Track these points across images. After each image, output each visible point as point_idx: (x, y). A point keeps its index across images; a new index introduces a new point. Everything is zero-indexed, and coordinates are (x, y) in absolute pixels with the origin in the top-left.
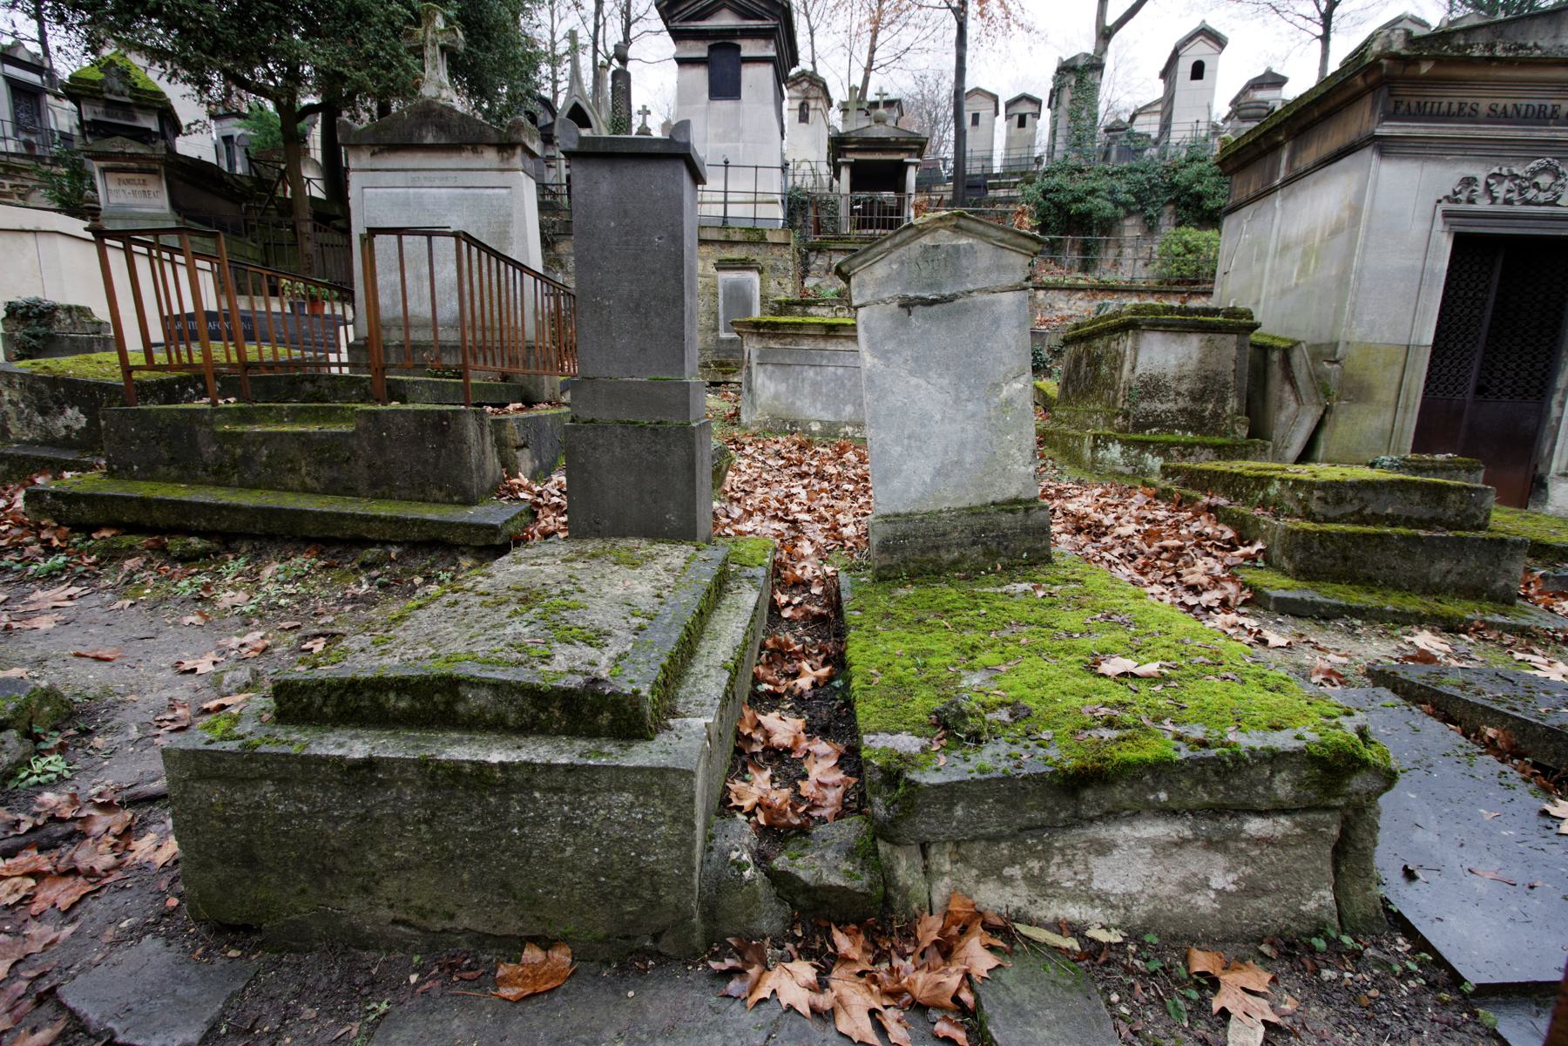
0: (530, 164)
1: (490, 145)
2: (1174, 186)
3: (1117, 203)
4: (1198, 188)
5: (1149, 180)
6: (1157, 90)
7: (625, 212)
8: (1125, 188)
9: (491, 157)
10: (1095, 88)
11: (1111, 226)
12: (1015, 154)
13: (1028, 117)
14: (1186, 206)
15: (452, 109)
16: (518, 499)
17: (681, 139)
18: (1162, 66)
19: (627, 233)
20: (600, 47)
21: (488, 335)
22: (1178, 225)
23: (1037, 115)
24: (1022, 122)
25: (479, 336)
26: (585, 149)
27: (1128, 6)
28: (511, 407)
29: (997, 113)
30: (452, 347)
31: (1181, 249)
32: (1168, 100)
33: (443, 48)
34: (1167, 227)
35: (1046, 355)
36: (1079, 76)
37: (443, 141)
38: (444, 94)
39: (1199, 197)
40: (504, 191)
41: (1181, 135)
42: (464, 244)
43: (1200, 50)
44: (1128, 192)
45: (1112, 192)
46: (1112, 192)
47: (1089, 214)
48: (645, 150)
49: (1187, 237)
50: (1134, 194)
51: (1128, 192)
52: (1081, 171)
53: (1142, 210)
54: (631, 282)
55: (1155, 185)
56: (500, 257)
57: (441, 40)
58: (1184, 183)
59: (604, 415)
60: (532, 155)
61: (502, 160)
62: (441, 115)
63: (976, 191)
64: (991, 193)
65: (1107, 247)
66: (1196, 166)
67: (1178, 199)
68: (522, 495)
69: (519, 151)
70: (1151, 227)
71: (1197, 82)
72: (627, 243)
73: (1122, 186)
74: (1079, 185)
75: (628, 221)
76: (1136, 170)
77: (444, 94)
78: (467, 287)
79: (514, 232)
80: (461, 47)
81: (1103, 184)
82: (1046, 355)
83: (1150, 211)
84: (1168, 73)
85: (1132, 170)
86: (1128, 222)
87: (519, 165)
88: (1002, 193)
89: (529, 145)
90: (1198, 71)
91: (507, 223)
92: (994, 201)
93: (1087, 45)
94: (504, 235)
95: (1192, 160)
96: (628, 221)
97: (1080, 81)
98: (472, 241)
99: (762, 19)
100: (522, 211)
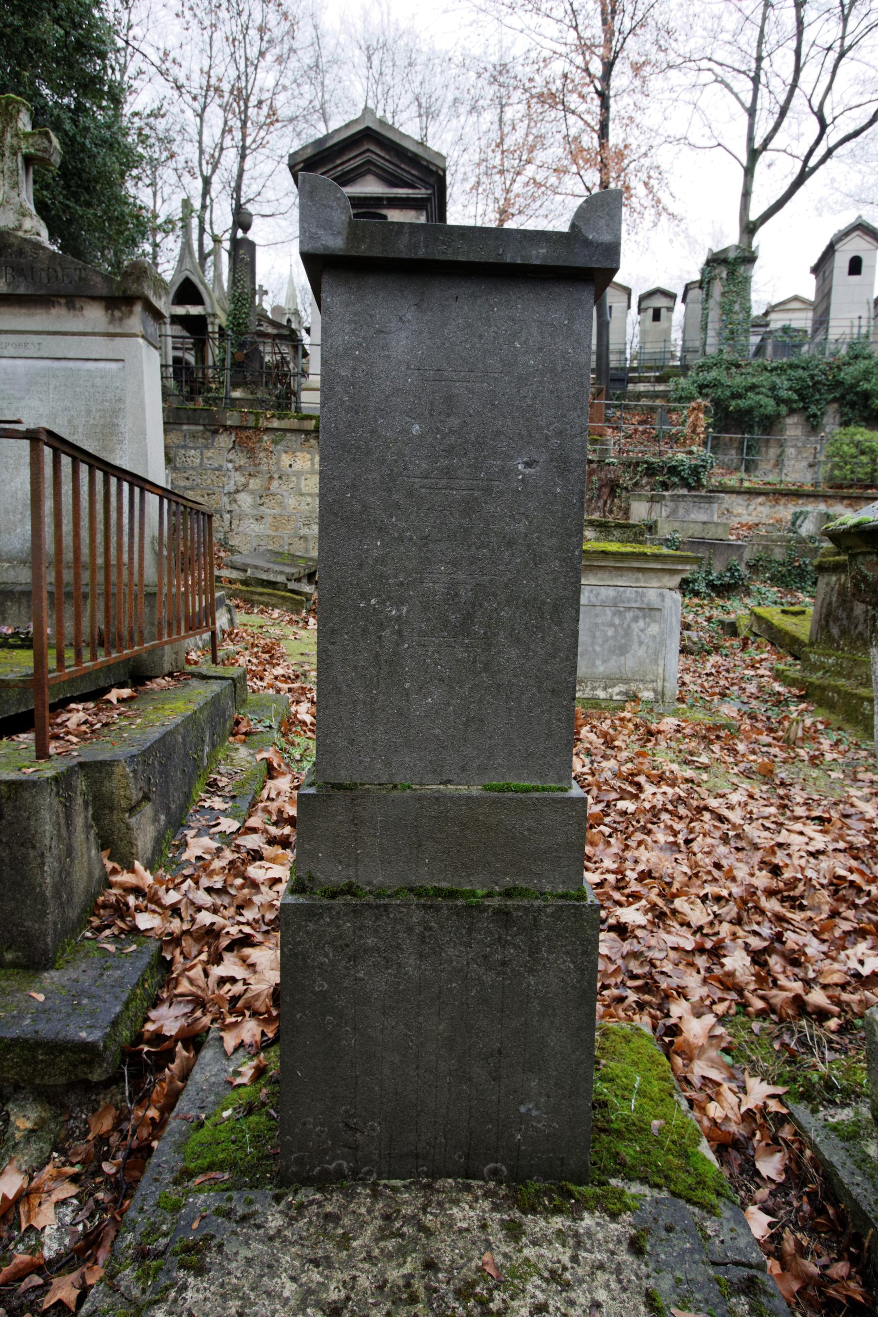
0: (152, 327)
1: (94, 298)
2: (838, 383)
3: (779, 401)
4: (866, 386)
5: (812, 377)
6: (808, 288)
7: (449, 400)
8: (786, 384)
9: (94, 316)
10: (747, 280)
11: (772, 424)
12: (649, 348)
13: (663, 312)
14: (852, 405)
15: (38, 246)
16: (134, 930)
17: (597, 235)
18: (814, 261)
19: (450, 451)
20: (207, 227)
21: (86, 576)
22: (845, 424)
23: (670, 309)
24: (657, 316)
25: (68, 576)
26: (363, 249)
27: (773, 201)
28: (113, 695)
29: (629, 307)
30: (23, 593)
31: (853, 450)
32: (825, 293)
33: (28, 160)
34: (831, 424)
35: (744, 571)
36: (730, 268)
37: (22, 291)
38: (28, 224)
39: (866, 396)
40: (113, 366)
41: (841, 331)
42: (48, 452)
43: (857, 245)
44: (790, 389)
45: (773, 388)
46: (773, 388)
47: (749, 411)
48: (510, 257)
49: (858, 437)
50: (796, 391)
51: (790, 389)
52: (738, 366)
53: (805, 409)
54: (455, 564)
55: (818, 382)
56: (110, 470)
57: (26, 148)
58: (849, 380)
59: (375, 875)
60: (157, 315)
61: (112, 320)
62: (21, 252)
63: (617, 385)
64: (631, 387)
65: (767, 447)
66: (862, 365)
67: (843, 397)
68: (144, 921)
69: (138, 308)
70: (813, 425)
71: (855, 278)
72: (448, 473)
73: (782, 382)
74: (739, 381)
75: (454, 422)
76: (797, 367)
77: (28, 224)
78: (48, 505)
79: (126, 425)
80: (56, 159)
81: (763, 379)
82: (744, 571)
83: (813, 409)
84: (822, 268)
85: (792, 366)
86: (790, 421)
87: (138, 329)
88: (642, 387)
89: (154, 300)
90: (856, 266)
91: (116, 413)
92: (639, 396)
93: (731, 237)
94: (109, 429)
95: (856, 357)
96: (454, 422)
97: (732, 274)
98: (61, 445)
99: (412, 187)
100: (139, 392)
